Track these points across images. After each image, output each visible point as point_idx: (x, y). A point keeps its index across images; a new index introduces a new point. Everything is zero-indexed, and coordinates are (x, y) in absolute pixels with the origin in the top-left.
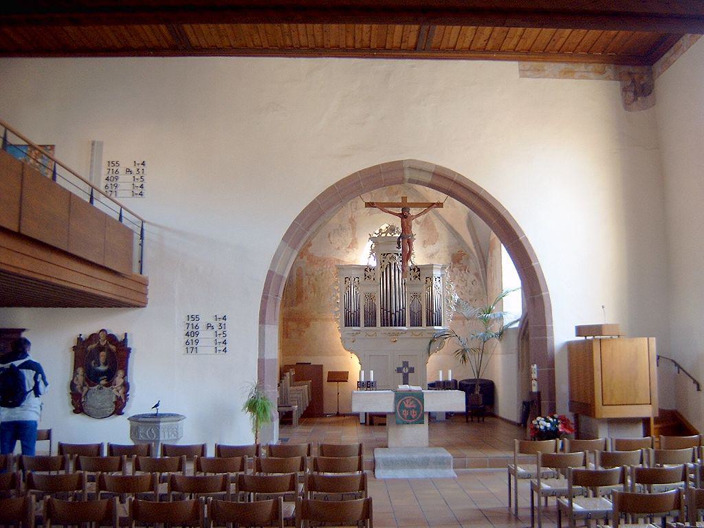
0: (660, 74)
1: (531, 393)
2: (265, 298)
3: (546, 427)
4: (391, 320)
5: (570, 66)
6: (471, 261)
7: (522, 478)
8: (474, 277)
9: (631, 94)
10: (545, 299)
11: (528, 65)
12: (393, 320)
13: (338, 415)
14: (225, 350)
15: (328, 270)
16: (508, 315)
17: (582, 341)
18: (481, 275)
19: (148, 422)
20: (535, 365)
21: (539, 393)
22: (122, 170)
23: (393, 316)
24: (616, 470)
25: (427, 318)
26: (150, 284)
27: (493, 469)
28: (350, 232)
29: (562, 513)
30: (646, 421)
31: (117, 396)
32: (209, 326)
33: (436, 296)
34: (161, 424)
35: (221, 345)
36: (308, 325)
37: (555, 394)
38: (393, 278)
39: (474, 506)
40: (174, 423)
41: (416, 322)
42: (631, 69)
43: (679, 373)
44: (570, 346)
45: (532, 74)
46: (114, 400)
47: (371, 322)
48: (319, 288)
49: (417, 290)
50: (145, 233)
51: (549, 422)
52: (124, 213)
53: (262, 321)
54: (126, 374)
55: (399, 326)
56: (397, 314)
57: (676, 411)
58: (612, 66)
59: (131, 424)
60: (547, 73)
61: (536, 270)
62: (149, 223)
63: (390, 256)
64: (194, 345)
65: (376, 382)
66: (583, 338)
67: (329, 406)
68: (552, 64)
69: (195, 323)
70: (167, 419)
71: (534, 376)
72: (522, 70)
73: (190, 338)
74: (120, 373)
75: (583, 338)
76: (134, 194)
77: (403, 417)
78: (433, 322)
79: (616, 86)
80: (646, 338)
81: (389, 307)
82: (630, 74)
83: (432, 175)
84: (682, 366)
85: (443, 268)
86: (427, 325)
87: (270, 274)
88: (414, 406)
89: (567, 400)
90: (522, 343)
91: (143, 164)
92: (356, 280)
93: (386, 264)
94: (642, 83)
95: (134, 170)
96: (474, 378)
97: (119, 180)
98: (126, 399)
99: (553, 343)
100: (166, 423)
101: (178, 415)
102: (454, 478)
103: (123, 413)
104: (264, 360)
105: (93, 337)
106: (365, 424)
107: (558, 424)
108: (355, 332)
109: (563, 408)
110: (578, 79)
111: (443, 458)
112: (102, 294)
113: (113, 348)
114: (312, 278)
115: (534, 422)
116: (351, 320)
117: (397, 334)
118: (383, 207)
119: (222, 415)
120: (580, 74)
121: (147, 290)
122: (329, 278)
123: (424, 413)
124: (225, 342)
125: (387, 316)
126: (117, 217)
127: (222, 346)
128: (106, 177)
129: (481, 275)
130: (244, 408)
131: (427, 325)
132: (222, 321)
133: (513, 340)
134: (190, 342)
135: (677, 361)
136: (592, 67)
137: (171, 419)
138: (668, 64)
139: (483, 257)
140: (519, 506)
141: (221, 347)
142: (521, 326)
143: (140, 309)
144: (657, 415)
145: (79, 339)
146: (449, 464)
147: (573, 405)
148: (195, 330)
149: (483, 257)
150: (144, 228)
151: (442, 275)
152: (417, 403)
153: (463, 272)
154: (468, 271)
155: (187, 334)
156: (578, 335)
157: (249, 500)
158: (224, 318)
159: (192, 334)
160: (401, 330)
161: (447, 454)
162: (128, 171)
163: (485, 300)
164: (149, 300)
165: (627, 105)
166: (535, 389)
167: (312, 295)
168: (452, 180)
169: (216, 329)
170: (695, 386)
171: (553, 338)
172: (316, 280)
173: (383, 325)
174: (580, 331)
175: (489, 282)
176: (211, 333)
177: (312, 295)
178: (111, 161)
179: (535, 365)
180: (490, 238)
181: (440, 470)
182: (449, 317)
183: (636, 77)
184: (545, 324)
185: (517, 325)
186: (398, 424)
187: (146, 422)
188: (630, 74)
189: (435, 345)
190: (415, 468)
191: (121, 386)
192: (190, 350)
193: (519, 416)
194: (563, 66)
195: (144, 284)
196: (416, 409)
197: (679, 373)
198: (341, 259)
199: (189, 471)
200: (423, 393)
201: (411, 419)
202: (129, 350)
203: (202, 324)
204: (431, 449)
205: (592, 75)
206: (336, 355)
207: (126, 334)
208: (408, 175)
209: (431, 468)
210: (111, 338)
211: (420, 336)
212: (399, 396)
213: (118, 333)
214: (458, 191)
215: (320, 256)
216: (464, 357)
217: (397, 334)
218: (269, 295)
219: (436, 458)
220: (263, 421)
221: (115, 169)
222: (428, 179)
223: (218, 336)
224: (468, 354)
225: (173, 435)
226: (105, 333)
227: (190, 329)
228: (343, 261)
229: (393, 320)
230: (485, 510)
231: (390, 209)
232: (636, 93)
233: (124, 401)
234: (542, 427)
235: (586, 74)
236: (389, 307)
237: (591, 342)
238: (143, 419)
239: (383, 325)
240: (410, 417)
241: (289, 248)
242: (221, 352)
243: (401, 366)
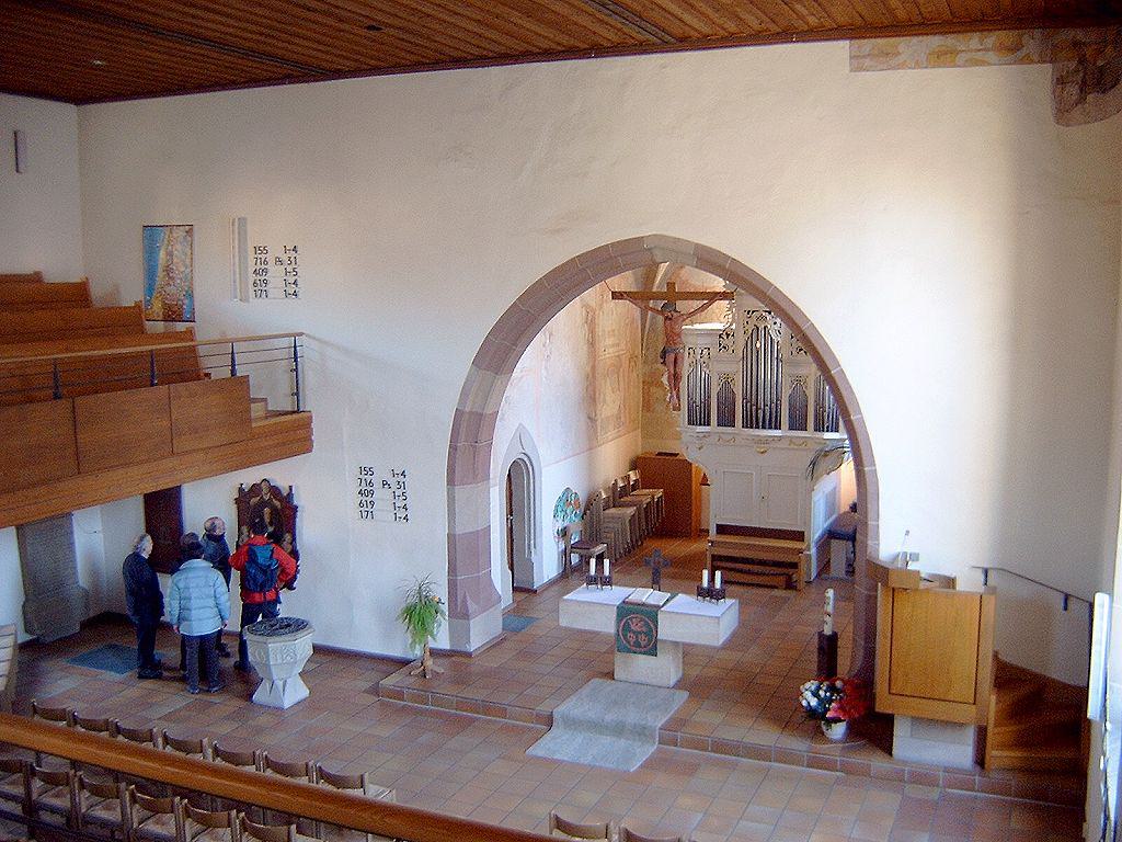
2: (453, 448)
11: (868, 45)
23: (760, 412)
25: (816, 416)
41: (798, 423)
42: (1080, 35)
45: (872, 63)
47: (727, 420)
58: (1037, 33)
60: (901, 59)
68: (915, 40)
82: (1076, 44)
87: (459, 414)
88: (644, 629)
91: (295, 249)
93: (750, 328)
94: (1100, 63)
95: (284, 258)
104: (454, 535)
105: (255, 489)
108: (701, 435)
110: (965, 66)
113: (277, 503)
117: (767, 440)
124: (405, 507)
127: (402, 513)
145: (241, 490)
152: (647, 624)
159: (366, 493)
165: (1063, 113)
176: (387, 493)
183: (1089, 52)
189: (823, 465)
192: (365, 514)
202: (295, 509)
205: (992, 56)
210: (275, 491)
213: (282, 483)
229: (768, 418)
232: (1084, 89)
234: (804, 703)
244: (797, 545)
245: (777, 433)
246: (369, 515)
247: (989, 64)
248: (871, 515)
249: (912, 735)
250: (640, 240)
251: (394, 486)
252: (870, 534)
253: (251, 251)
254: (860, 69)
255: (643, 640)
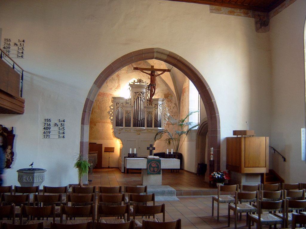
0: (273, 17)
1: (210, 160)
2: (84, 111)
3: (218, 177)
4: (138, 124)
5: (233, 9)
6: (173, 97)
7: (221, 203)
8: (174, 105)
9: (259, 25)
10: (217, 117)
12: (119, 122)
13: (109, 168)
14: (64, 137)
15: (106, 99)
16: (193, 123)
17: (235, 137)
18: (177, 104)
19: (27, 173)
20: (213, 148)
21: (213, 161)
22: (12, 44)
23: (139, 122)
24: (280, 202)
26: (25, 102)
27: (195, 196)
28: (117, 81)
29: (250, 220)
30: (262, 175)
31: (7, 159)
32: (56, 125)
33: (159, 113)
34: (35, 174)
35: (62, 134)
36: (95, 125)
37: (220, 161)
38: (139, 104)
39: (195, 216)
40: (41, 173)
41: (149, 125)
42: (260, 13)
43: (275, 153)
44: (228, 139)
46: (6, 161)
47: (128, 125)
48: (101, 107)
49: (151, 110)
50: (24, 76)
51: (220, 174)
52: (15, 66)
53: (83, 123)
54: (12, 148)
55: (142, 127)
56: (141, 121)
57: (272, 170)
59: (18, 173)
60: (221, 12)
61: (214, 104)
62: (26, 71)
63: (139, 93)
64: (48, 134)
65: (137, 154)
66: (236, 136)
67: (104, 164)
69: (49, 123)
70: (38, 172)
71: (212, 153)
72: (211, 9)
73: (46, 131)
74: (9, 147)
75: (236, 136)
76: (18, 56)
77: (151, 171)
78: (119, 125)
79: (252, 20)
80: (265, 137)
81: (137, 117)
82: (259, 15)
83: (167, 56)
84: (276, 149)
85: (163, 101)
86: (155, 127)
89: (225, 164)
90: (199, 137)
91: (23, 41)
92: (122, 104)
95: (19, 44)
96: (175, 152)
97: (10, 49)
98: (12, 160)
99: (220, 137)
100: (37, 174)
101: (42, 169)
102: (178, 201)
103: (10, 168)
106: (124, 173)
107: (223, 175)
109: (223, 168)
111: (171, 191)
112: (5, 107)
113: (6, 134)
114: (98, 102)
115: (212, 174)
116: (118, 123)
117: (141, 130)
118: (142, 70)
119: (61, 169)
120: (237, 13)
121: (24, 106)
122: (106, 103)
123: (160, 169)
124: (64, 133)
125: (136, 122)
126: (12, 67)
127: (62, 135)
128: (3, 47)
129: (177, 104)
130: (75, 166)
131: (155, 127)
132: (62, 122)
133: (194, 136)
134: (46, 132)
135: (274, 148)
136: (242, 11)
137: (39, 171)
138: (278, 12)
139: (179, 97)
140: (220, 215)
141: (62, 135)
142: (199, 128)
143: (21, 115)
144: (268, 172)
146: (174, 193)
147: (228, 166)
148: (49, 127)
149: (179, 97)
150: (24, 74)
151: (162, 104)
153: (169, 102)
154: (172, 102)
155: (44, 128)
156: (234, 135)
157: (40, 205)
158: (64, 121)
159: (47, 129)
160: (141, 129)
161: (173, 189)
162: (16, 44)
163: (179, 116)
164: (25, 111)
165: (257, 30)
166: (212, 159)
167: (98, 110)
168: (176, 59)
169: (59, 126)
170: (283, 160)
171: (220, 136)
172: (100, 103)
173: (134, 126)
174: (235, 133)
175: (181, 108)
176: (56, 128)
177: (98, 110)
178: (6, 38)
179: (213, 148)
180: (182, 87)
181: (171, 197)
182: (165, 123)
184: (217, 128)
185: (197, 128)
186: (148, 174)
187: (26, 173)
188: (259, 15)
189: (158, 136)
190: (159, 196)
191: (10, 153)
192: (46, 136)
193: (196, 170)
194: (230, 9)
195: (23, 102)
196: (157, 167)
197: (275, 153)
198: (112, 94)
199: (64, 200)
200: (160, 160)
201: (155, 172)
202: (14, 136)
203: (52, 123)
204: (164, 186)
205: (242, 14)
206: (108, 140)
207: (13, 128)
208: (156, 55)
209: (166, 196)
211: (151, 132)
212: (149, 161)
214: (180, 65)
215: (102, 92)
216: (169, 142)
217: (141, 131)
218: (87, 110)
219: (168, 191)
220: (84, 172)
221: (8, 43)
222: (165, 57)
223: (60, 130)
224: (171, 142)
225: (40, 180)
226: (1, 126)
227: (46, 126)
228: (113, 95)
229: (119, 122)
230: (203, 218)
231: (145, 71)
233: (11, 161)
234: (216, 177)
235: (239, 14)
236: (137, 117)
237: (240, 138)
238: (26, 172)
239: (134, 126)
240: (154, 171)
241: (97, 87)
242: (62, 138)
243: (149, 146)
244: (30, 219)
245: (144, 128)
246: (48, 136)
247: (242, 16)
248: (218, 127)
249: (246, 182)
250: (153, 49)
251: (59, 126)
252: (218, 133)
253: (3, 40)
254: (212, 12)
255: (156, 170)
